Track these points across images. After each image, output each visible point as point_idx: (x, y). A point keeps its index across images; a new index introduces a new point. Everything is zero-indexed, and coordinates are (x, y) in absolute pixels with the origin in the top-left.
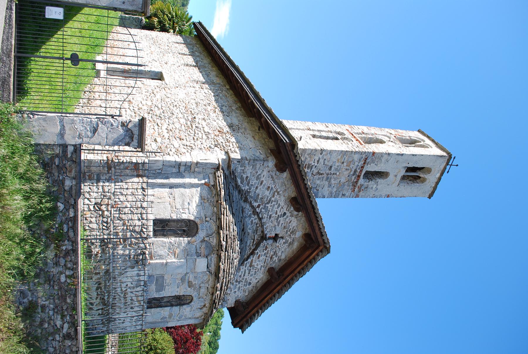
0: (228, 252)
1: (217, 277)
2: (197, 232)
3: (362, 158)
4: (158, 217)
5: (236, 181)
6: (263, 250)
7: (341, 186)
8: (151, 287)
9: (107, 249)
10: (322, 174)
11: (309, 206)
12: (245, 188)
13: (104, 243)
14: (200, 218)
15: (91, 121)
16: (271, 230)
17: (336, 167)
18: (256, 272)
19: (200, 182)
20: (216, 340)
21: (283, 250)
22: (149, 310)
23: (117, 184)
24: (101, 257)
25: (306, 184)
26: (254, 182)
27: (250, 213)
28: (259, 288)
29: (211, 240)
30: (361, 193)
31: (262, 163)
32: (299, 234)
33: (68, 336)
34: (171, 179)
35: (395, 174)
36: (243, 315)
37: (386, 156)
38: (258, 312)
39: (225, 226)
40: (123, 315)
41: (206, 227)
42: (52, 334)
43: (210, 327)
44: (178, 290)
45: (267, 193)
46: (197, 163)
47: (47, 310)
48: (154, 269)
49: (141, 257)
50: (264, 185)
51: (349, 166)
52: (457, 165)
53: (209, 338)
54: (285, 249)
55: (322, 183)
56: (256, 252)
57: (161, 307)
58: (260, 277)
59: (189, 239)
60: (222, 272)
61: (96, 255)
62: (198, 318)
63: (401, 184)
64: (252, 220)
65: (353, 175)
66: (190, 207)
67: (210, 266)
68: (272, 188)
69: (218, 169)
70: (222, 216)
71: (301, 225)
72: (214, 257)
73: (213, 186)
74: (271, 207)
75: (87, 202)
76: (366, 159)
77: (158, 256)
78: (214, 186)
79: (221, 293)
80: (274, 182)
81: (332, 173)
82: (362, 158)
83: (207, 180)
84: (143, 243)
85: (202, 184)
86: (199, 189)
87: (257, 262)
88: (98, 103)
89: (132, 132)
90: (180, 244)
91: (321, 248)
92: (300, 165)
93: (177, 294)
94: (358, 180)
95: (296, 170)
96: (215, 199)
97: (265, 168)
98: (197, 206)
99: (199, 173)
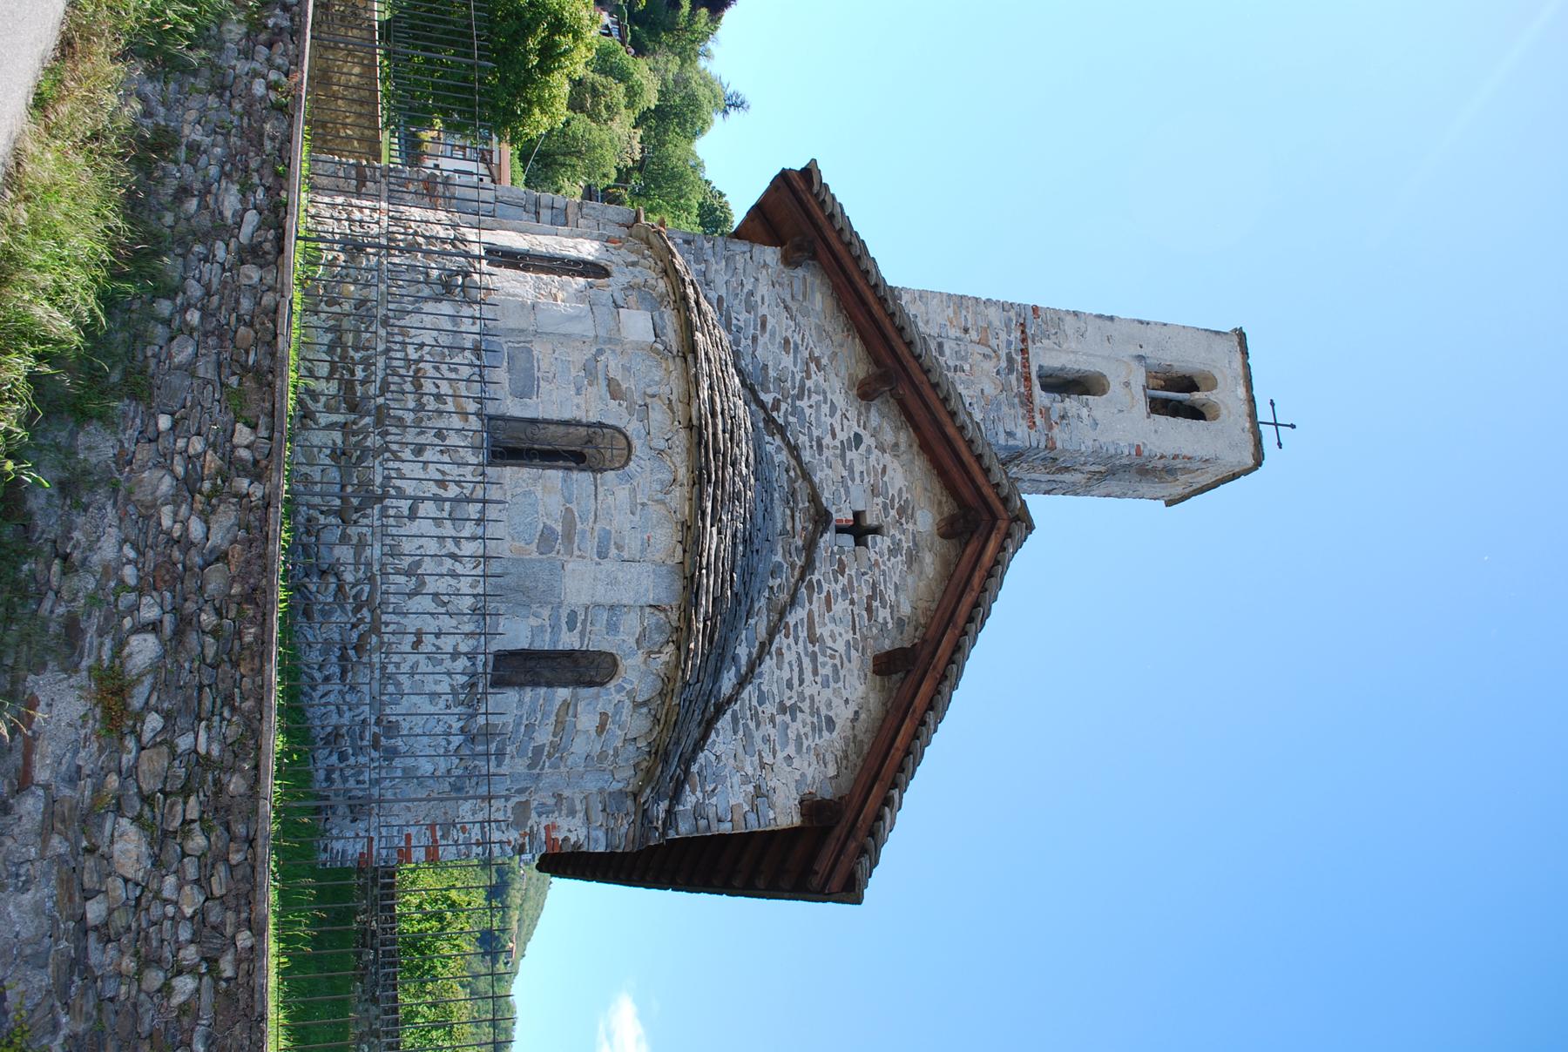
28: (866, 748)
30: (1056, 430)
33: (251, 253)
37: (1069, 318)
42: (206, 237)
45: (787, 360)
47: (204, 159)
50: (773, 335)
68: (796, 345)
74: (812, 411)
87: (831, 626)
91: (1002, 525)
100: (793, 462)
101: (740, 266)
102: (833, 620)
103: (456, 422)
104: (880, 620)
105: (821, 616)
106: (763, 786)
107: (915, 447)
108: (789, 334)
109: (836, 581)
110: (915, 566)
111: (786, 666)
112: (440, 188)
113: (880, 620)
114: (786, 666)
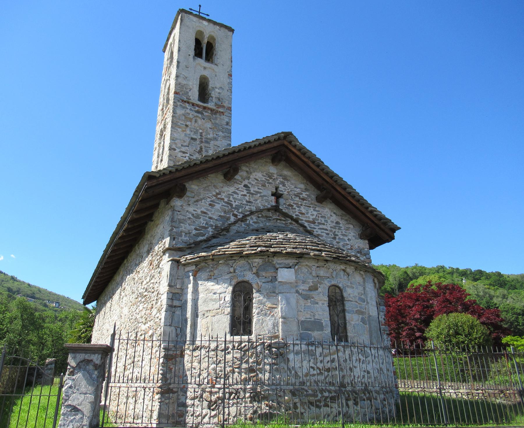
0: (273, 244)
1: (301, 256)
2: (247, 282)
3: (181, 105)
4: (228, 330)
5: (201, 241)
6: (292, 209)
7: (216, 127)
8: (317, 337)
9: (263, 393)
10: (201, 148)
11: (231, 157)
12: (211, 231)
13: (256, 397)
14: (231, 279)
15: (64, 414)
16: (267, 201)
17: (192, 133)
18: (322, 217)
19: (192, 282)
20: (471, 273)
21: (293, 187)
22: (349, 339)
23: (189, 381)
24: (273, 401)
25: (201, 162)
26: (203, 222)
27: (243, 225)
28: (344, 213)
29: (256, 264)
30: (225, 105)
31: (176, 213)
32: (273, 170)
34: (187, 316)
35: (202, 69)
36: (379, 231)
38: (371, 212)
39: (238, 249)
40: (357, 372)
41: (241, 271)
43: (456, 279)
44: (320, 303)
45: (218, 206)
46: (170, 285)
48: (290, 333)
49: (274, 349)
50: (208, 210)
51: (192, 119)
52: (200, 6)
53: (468, 281)
54: (292, 184)
55: (212, 148)
56: (295, 217)
57: (345, 324)
58: (329, 211)
59: (254, 291)
60: (295, 250)
61: (270, 407)
62: (364, 279)
63: (216, 62)
64: (254, 222)
65: (202, 114)
66: (218, 292)
67: (289, 264)
68: (211, 201)
69: (178, 262)
70: (226, 253)
71: (260, 167)
72: (277, 261)
73: (196, 266)
74: (237, 201)
75: (206, 420)
76: (183, 101)
77: (274, 328)
78: (196, 264)
79: (325, 251)
80: (204, 198)
81: (199, 137)
82: (181, 105)
83: (191, 274)
84: (257, 346)
85: (195, 280)
86: (200, 282)
87: (309, 215)
88: (122, 407)
89: (82, 362)
90: (260, 302)
91: (286, 143)
92: (177, 170)
93: (326, 304)
94: (209, 109)
95: (183, 173)
96: (210, 262)
97: (184, 210)
98: (218, 283)
99: (183, 283)
100: (256, 214)
101: (182, 217)
102: (307, 213)
103: (340, 354)
104: (306, 196)
105: (306, 217)
106: (357, 250)
107: (247, 164)
108: (208, 203)
109: (295, 209)
110: (288, 178)
111: (322, 234)
112: (171, 353)
113: (306, 196)
114: (322, 234)
